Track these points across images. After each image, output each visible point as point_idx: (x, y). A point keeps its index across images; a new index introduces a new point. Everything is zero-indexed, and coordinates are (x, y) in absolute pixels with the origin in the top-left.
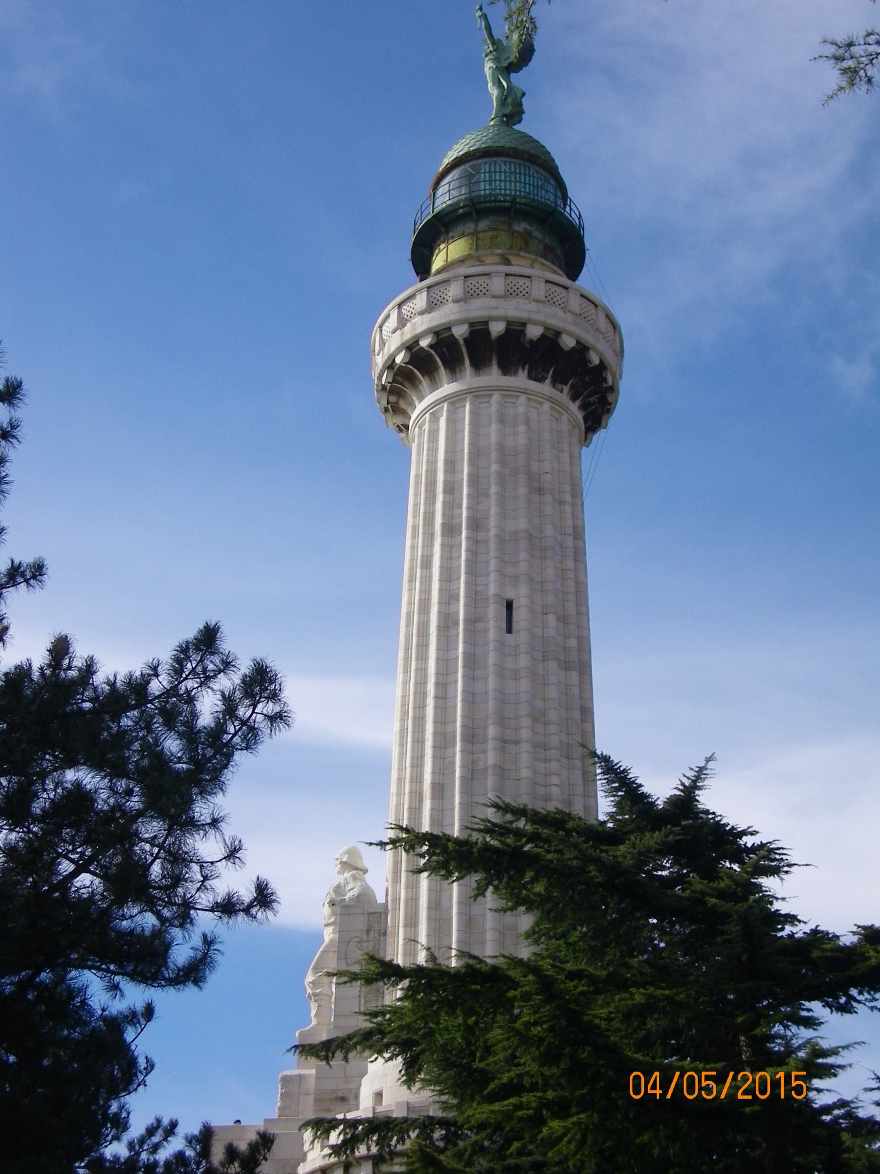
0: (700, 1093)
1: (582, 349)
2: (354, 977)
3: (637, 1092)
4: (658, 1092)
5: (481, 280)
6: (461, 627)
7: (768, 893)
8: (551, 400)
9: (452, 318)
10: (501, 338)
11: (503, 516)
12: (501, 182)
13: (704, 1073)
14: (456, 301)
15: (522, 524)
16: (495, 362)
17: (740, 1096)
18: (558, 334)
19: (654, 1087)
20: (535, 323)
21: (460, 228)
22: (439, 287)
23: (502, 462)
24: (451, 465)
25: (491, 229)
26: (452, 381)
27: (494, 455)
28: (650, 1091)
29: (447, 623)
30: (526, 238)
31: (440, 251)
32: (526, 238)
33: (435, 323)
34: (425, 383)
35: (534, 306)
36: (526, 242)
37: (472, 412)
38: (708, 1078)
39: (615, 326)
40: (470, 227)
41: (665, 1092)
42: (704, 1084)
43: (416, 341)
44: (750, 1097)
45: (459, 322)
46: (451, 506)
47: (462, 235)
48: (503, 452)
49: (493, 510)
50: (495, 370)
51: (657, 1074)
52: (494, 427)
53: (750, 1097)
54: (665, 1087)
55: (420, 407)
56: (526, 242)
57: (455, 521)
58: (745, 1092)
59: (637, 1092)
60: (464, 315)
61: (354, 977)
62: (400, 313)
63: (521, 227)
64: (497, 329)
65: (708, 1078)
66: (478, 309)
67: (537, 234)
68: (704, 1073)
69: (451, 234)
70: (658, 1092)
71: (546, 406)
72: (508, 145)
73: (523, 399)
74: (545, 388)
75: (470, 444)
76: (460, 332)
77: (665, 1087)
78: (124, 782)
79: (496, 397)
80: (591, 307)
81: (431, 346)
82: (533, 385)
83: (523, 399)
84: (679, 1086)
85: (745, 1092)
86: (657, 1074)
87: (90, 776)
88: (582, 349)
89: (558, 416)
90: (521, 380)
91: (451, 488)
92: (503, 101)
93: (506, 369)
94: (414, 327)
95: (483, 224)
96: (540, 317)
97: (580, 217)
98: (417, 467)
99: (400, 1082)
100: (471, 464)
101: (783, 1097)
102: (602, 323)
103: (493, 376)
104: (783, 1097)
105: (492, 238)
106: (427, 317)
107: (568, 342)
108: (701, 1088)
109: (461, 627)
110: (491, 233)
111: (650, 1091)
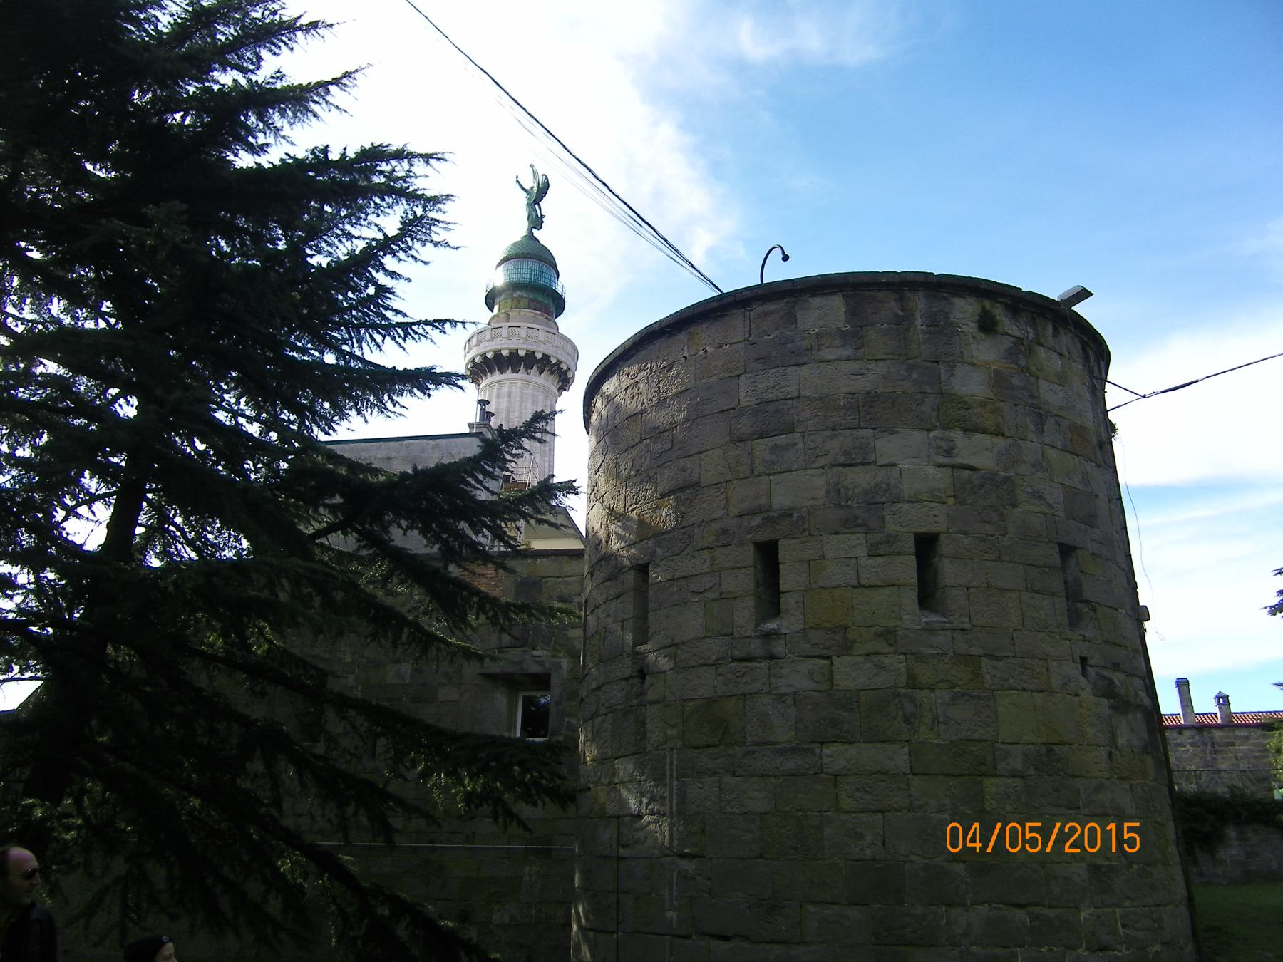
0: (1023, 847)
2: (582, 791)
3: (954, 845)
4: (978, 845)
7: (351, 662)
13: (1028, 825)
17: (1067, 850)
19: (973, 840)
38: (1032, 829)
41: (986, 845)
42: (1028, 836)
44: (1078, 851)
51: (976, 825)
53: (1078, 851)
54: (985, 841)
58: (1072, 846)
59: (954, 845)
61: (582, 791)
65: (1032, 829)
68: (1028, 825)
70: (978, 845)
77: (985, 841)
78: (310, 590)
82: (503, 377)
84: (1001, 836)
85: (1072, 846)
86: (976, 825)
87: (383, 641)
89: (910, 362)
99: (285, 157)
101: (1114, 850)
102: (569, 348)
104: (1114, 850)
108: (1024, 841)
111: (969, 844)
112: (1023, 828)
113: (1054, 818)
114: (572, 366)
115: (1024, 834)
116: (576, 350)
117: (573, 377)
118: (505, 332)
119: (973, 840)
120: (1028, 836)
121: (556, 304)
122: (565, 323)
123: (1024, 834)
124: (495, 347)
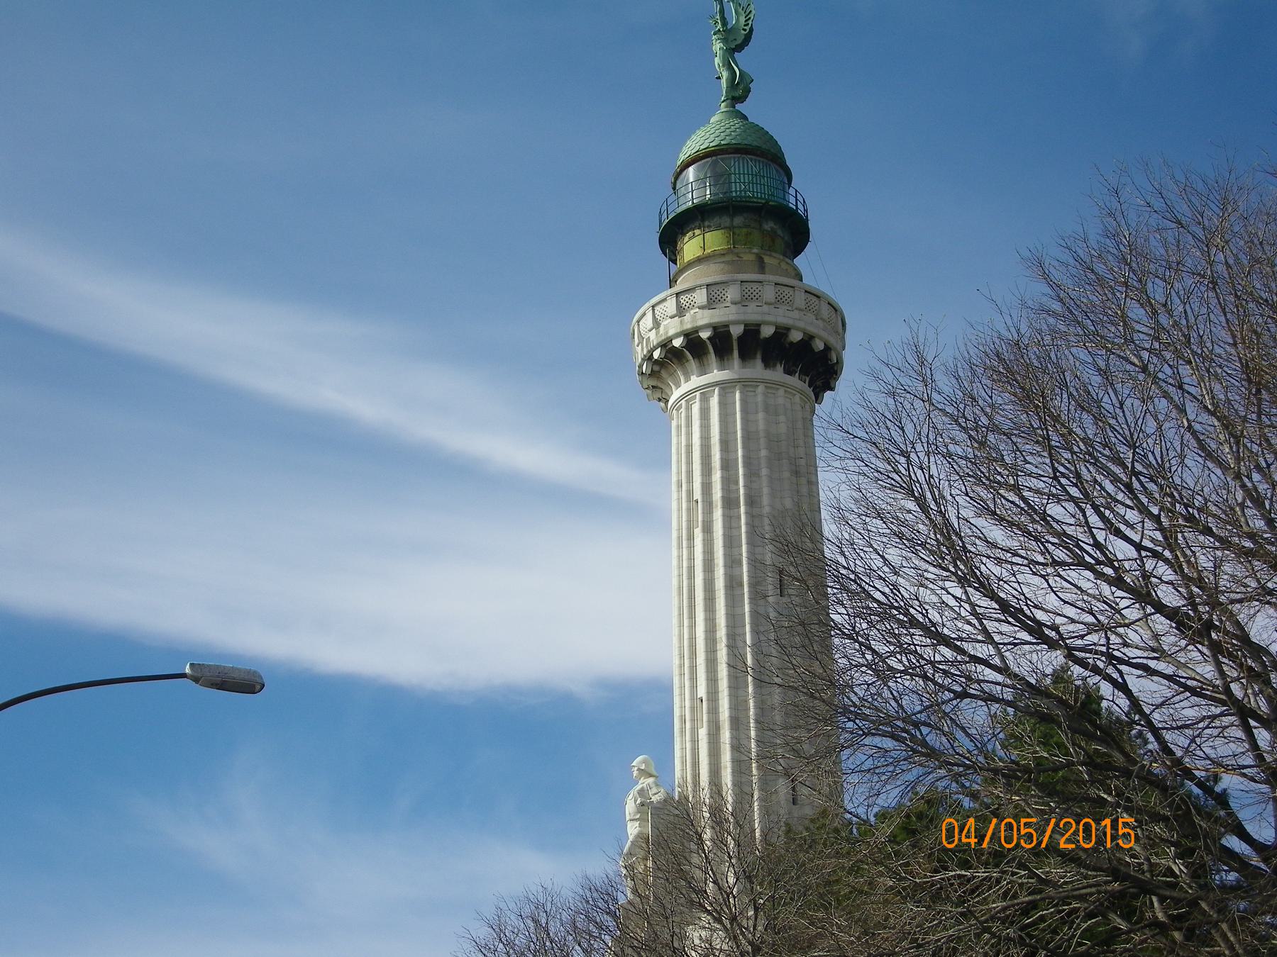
1: (808, 339)
4: (973, 841)
5: (755, 286)
6: (746, 589)
8: (801, 392)
9: (732, 318)
10: (768, 340)
11: (773, 495)
12: (746, 181)
13: (1023, 821)
14: (734, 303)
15: (788, 503)
16: (759, 356)
18: (812, 337)
20: (798, 329)
21: (716, 220)
22: (718, 287)
23: (769, 448)
24: (726, 445)
25: (746, 226)
26: (722, 368)
27: (762, 441)
28: (964, 840)
29: (733, 584)
30: (773, 235)
31: (694, 236)
32: (773, 235)
33: (716, 320)
34: (692, 364)
35: (796, 314)
36: (773, 241)
37: (742, 400)
39: (844, 325)
40: (726, 220)
41: (980, 842)
42: (1023, 832)
43: (696, 330)
45: (736, 323)
46: (729, 481)
47: (718, 228)
48: (772, 441)
49: (766, 490)
50: (759, 363)
51: (972, 820)
52: (761, 415)
54: (981, 838)
55: (685, 387)
56: (773, 241)
57: (732, 496)
60: (742, 317)
62: (678, 302)
63: (769, 225)
64: (767, 331)
66: (753, 313)
67: (780, 232)
68: (1023, 821)
69: (707, 223)
71: (797, 398)
72: (755, 143)
73: (781, 391)
74: (794, 381)
75: (742, 429)
76: (736, 331)
77: (981, 838)
79: (761, 389)
80: (814, 299)
81: (709, 338)
82: (789, 379)
83: (781, 391)
88: (808, 339)
90: (777, 374)
91: (727, 465)
92: (732, 85)
93: (768, 363)
94: (694, 318)
95: (738, 220)
96: (801, 325)
97: (806, 210)
98: (677, 442)
100: (744, 447)
102: (826, 311)
103: (757, 369)
105: (747, 234)
106: (707, 312)
107: (819, 345)
109: (746, 589)
110: (745, 230)
111: (964, 840)
112: (1018, 822)
113: (1095, 850)
114: (832, 341)
115: (1019, 830)
116: (834, 308)
117: (839, 362)
118: (769, 293)
119: (968, 837)
120: (1023, 832)
121: (794, 232)
122: (812, 265)
123: (1019, 830)
124: (782, 320)
